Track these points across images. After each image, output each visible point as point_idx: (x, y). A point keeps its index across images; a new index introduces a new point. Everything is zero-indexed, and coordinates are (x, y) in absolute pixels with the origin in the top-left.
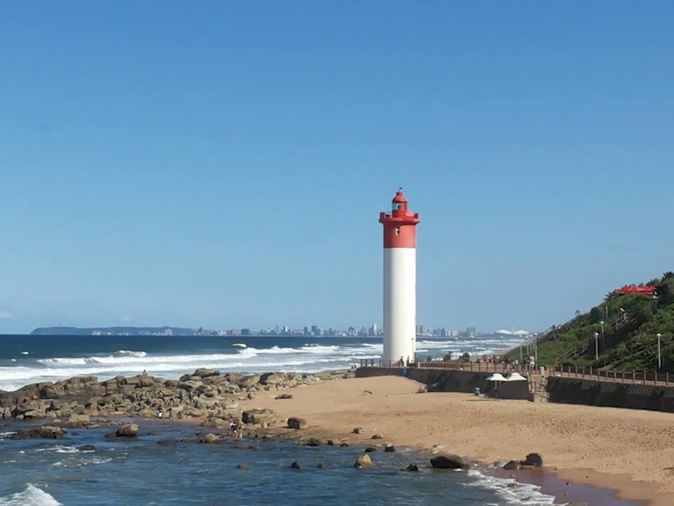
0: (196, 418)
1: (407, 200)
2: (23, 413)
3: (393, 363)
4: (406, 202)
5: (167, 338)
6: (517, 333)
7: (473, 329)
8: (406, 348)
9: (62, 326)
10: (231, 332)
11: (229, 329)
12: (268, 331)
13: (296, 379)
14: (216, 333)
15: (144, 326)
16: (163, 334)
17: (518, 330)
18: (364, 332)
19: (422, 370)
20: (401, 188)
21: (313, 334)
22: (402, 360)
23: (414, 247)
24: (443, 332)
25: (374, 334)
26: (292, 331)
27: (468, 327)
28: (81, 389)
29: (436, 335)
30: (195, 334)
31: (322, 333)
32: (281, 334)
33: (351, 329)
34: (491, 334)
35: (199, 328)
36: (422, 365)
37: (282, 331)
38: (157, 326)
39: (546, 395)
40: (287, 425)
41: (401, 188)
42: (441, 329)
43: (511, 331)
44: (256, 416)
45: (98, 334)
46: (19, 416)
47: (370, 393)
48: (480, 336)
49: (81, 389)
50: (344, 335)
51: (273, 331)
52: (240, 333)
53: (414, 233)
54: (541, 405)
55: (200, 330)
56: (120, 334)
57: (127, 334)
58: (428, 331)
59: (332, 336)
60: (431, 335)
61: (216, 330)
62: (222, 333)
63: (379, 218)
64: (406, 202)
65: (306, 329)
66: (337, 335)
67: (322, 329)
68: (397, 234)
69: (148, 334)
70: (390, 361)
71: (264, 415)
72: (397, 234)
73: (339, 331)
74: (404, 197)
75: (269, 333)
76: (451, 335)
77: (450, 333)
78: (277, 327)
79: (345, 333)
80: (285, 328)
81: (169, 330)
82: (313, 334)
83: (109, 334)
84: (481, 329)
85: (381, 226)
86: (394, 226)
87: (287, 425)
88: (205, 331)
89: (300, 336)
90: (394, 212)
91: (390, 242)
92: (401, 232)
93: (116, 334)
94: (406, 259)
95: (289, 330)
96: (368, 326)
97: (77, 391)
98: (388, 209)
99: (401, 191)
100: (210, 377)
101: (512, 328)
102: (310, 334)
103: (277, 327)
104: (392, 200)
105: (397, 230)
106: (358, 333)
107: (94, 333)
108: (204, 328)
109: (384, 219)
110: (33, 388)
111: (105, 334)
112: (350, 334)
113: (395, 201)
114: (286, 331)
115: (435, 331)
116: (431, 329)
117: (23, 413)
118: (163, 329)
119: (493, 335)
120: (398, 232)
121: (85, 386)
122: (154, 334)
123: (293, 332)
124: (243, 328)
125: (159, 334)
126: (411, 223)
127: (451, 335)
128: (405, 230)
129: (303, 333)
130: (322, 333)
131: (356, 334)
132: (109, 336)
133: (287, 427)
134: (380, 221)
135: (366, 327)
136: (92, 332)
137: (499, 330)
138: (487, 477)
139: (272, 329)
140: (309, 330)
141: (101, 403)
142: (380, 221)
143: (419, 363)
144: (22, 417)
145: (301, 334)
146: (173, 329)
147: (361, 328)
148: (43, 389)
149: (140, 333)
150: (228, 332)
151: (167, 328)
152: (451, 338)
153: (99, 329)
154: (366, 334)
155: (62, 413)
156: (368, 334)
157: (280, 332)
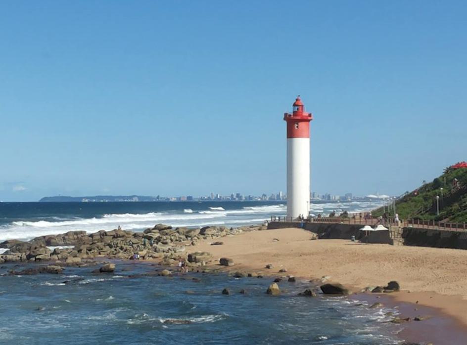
2: (35, 256)
3: (294, 219)
4: (302, 106)
5: (136, 203)
7: (350, 195)
8: (303, 208)
9: (61, 195)
11: (179, 197)
12: (206, 198)
14: (169, 199)
16: (132, 201)
17: (382, 194)
18: (273, 198)
19: (314, 223)
20: (299, 96)
21: (237, 199)
23: (308, 137)
24: (329, 197)
25: (280, 199)
30: (154, 200)
32: (214, 199)
34: (363, 198)
35: (157, 196)
36: (314, 220)
38: (128, 195)
39: (402, 240)
40: (219, 263)
41: (299, 96)
43: (377, 195)
45: (87, 201)
49: (75, 239)
50: (259, 200)
51: (209, 197)
52: (186, 199)
54: (399, 247)
55: (158, 197)
56: (102, 201)
57: (107, 201)
58: (318, 196)
59: (251, 201)
60: (320, 199)
62: (173, 200)
63: (283, 117)
64: (302, 106)
65: (232, 195)
66: (254, 200)
68: (296, 128)
70: (292, 218)
71: (203, 256)
72: (296, 128)
74: (301, 102)
75: (206, 199)
76: (335, 198)
77: (334, 198)
79: (260, 198)
80: (217, 195)
82: (237, 199)
83: (94, 201)
85: (285, 123)
86: (294, 122)
87: (219, 263)
88: (161, 198)
89: (228, 200)
90: (295, 113)
94: (303, 146)
95: (221, 197)
97: (72, 241)
98: (290, 111)
99: (299, 98)
100: (165, 230)
102: (235, 199)
103: (212, 194)
104: (293, 104)
105: (296, 125)
106: (269, 198)
107: (84, 201)
108: (161, 196)
109: (287, 117)
111: (91, 201)
112: (263, 199)
113: (295, 105)
114: (219, 197)
115: (323, 196)
116: (320, 195)
117: (35, 256)
118: (131, 197)
119: (364, 199)
121: (78, 237)
122: (126, 201)
124: (188, 196)
125: (129, 201)
126: (307, 120)
128: (302, 125)
129: (230, 199)
130: (244, 199)
134: (285, 119)
137: (369, 194)
139: (208, 196)
140: (234, 197)
149: (116, 200)
150: (177, 198)
151: (135, 196)
153: (87, 198)
154: (274, 199)
156: (276, 198)
157: (214, 198)
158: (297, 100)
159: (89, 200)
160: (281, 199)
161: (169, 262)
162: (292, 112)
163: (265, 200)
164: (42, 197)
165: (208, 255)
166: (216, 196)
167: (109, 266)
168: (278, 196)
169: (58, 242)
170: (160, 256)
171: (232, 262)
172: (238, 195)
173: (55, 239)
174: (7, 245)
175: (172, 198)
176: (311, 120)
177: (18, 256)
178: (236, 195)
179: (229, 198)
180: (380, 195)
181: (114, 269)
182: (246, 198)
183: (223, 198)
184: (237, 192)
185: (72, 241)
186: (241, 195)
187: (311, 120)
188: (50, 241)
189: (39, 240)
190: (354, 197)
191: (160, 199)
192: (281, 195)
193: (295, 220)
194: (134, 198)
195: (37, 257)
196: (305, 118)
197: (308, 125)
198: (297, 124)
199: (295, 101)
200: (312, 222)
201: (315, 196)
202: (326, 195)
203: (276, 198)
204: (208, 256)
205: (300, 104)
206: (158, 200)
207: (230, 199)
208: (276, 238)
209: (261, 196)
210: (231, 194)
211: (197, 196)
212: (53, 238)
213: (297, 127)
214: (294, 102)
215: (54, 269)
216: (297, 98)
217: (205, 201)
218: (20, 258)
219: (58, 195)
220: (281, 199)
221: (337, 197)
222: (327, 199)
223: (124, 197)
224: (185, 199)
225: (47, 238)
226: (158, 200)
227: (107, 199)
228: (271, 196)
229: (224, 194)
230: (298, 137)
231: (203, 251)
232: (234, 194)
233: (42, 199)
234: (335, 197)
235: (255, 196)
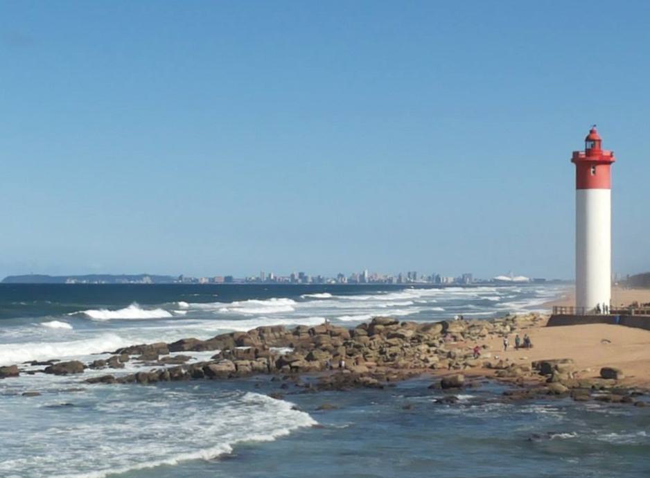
0: (473, 368)
1: (601, 138)
2: (289, 363)
3: (585, 312)
4: (599, 141)
6: (516, 279)
7: (470, 276)
8: (602, 295)
9: (34, 274)
10: (213, 279)
11: (213, 277)
12: (253, 278)
13: (486, 328)
14: (197, 280)
15: (121, 274)
16: (141, 282)
17: (519, 275)
18: (353, 279)
19: (637, 317)
20: (595, 126)
21: (300, 281)
22: (598, 307)
23: (609, 188)
24: (438, 278)
25: (364, 281)
26: (278, 278)
27: (464, 273)
28: (276, 338)
29: (431, 282)
30: (175, 282)
31: (310, 280)
32: (266, 281)
33: (341, 276)
34: (489, 280)
35: (179, 275)
36: (637, 312)
37: (267, 278)
38: (135, 274)
40: (599, 375)
41: (595, 126)
42: (437, 274)
43: (510, 277)
44: (560, 366)
45: (73, 282)
46: (285, 367)
47: (609, 342)
48: (478, 283)
49: (276, 338)
50: (333, 282)
51: (258, 278)
52: (223, 281)
53: (609, 171)
55: (181, 278)
56: (96, 282)
57: (103, 282)
58: (422, 278)
59: (321, 284)
60: (425, 282)
61: (197, 278)
62: (204, 281)
63: (571, 157)
64: (599, 141)
65: (293, 276)
66: (325, 283)
67: (310, 277)
68: (592, 174)
69: (125, 281)
70: (583, 308)
71: (566, 365)
72: (592, 174)
73: (328, 279)
74: (598, 135)
75: (253, 281)
76: (447, 281)
77: (445, 280)
78: (262, 274)
79: (335, 280)
80: (270, 275)
81: (148, 278)
82: (300, 281)
83: (84, 282)
84: (477, 276)
85: (573, 167)
86: (588, 166)
87: (599, 375)
88: (186, 279)
89: (287, 283)
90: (588, 152)
91: (583, 182)
92: (596, 172)
93: (91, 283)
94: (601, 200)
95: (275, 278)
96: (358, 273)
97: (273, 341)
99: (595, 129)
100: (391, 326)
101: (512, 273)
102: (297, 281)
103: (262, 274)
104: (585, 138)
105: (592, 170)
106: (348, 280)
107: (68, 282)
108: (185, 276)
109: (576, 158)
110: (228, 338)
111: (80, 282)
112: (340, 281)
113: (588, 139)
114: (272, 277)
115: (429, 277)
116: (424, 276)
117: (289, 363)
119: (491, 282)
120: (594, 172)
121: (281, 335)
122: (132, 282)
123: (279, 280)
124: (227, 275)
125: (137, 282)
126: (607, 162)
127: (447, 281)
128: (601, 169)
129: (290, 280)
130: (310, 280)
131: (346, 282)
132: (95, 284)
133: (599, 377)
134: (573, 161)
135: (356, 273)
136: (66, 281)
137: (497, 276)
138: (233, 393)
139: (257, 276)
140: (296, 277)
141: (350, 353)
142: (573, 161)
143: (633, 310)
144: (288, 367)
145: (288, 281)
146: (151, 277)
147: (351, 275)
148: (238, 339)
149: (117, 281)
150: (210, 279)
151: (145, 275)
152: (447, 284)
153: (74, 277)
154: (356, 281)
155: (321, 363)
156: (358, 280)
157: (265, 279)
158: (592, 132)
159: (76, 280)
160: (367, 281)
161: (516, 373)
162: (584, 149)
163: (342, 282)
164: (6, 276)
165: (573, 363)
166: (267, 276)
167: (457, 377)
168: (362, 276)
169: (254, 342)
170: (478, 365)
171: (621, 373)
172: (301, 275)
173: (250, 338)
174: (184, 345)
175: (202, 279)
176: (613, 161)
177: (264, 363)
178: (298, 275)
179: (287, 279)
180: (515, 276)
181: (463, 382)
182: (313, 278)
183: (279, 280)
184: (301, 271)
185: (273, 341)
186: (305, 275)
187: (613, 161)
188: (242, 340)
189: (224, 338)
190: (475, 280)
191: (183, 280)
192: (366, 275)
193: (592, 311)
194: (144, 279)
195: (294, 364)
196: (604, 159)
197: (609, 169)
198: (594, 168)
199: (589, 133)
200: (633, 314)
201: (417, 278)
202: (433, 276)
203: (358, 280)
204: (573, 365)
205: (597, 138)
206: (180, 281)
207: (290, 280)
208: (606, 339)
209: (336, 277)
210: (291, 273)
211: (241, 274)
212: (246, 337)
213: (594, 172)
214: (587, 135)
215: (368, 381)
216: (591, 129)
217: (251, 283)
218: (266, 366)
219: (29, 274)
220: (367, 281)
221: (451, 280)
222: (434, 282)
223: (129, 277)
224: (221, 281)
225: (236, 337)
226: (180, 281)
227: (103, 280)
228: (351, 277)
229: (282, 272)
230: (591, 188)
231: (565, 357)
232: (295, 273)
233: (5, 279)
234: (447, 279)
235: (326, 277)
